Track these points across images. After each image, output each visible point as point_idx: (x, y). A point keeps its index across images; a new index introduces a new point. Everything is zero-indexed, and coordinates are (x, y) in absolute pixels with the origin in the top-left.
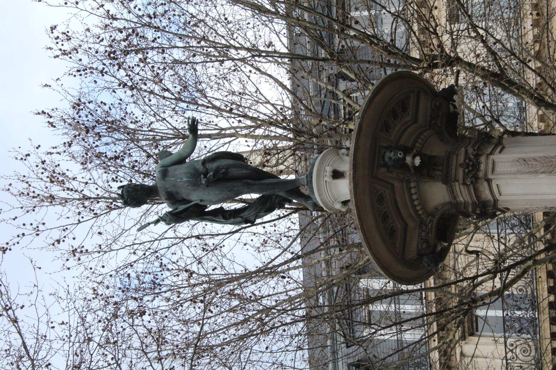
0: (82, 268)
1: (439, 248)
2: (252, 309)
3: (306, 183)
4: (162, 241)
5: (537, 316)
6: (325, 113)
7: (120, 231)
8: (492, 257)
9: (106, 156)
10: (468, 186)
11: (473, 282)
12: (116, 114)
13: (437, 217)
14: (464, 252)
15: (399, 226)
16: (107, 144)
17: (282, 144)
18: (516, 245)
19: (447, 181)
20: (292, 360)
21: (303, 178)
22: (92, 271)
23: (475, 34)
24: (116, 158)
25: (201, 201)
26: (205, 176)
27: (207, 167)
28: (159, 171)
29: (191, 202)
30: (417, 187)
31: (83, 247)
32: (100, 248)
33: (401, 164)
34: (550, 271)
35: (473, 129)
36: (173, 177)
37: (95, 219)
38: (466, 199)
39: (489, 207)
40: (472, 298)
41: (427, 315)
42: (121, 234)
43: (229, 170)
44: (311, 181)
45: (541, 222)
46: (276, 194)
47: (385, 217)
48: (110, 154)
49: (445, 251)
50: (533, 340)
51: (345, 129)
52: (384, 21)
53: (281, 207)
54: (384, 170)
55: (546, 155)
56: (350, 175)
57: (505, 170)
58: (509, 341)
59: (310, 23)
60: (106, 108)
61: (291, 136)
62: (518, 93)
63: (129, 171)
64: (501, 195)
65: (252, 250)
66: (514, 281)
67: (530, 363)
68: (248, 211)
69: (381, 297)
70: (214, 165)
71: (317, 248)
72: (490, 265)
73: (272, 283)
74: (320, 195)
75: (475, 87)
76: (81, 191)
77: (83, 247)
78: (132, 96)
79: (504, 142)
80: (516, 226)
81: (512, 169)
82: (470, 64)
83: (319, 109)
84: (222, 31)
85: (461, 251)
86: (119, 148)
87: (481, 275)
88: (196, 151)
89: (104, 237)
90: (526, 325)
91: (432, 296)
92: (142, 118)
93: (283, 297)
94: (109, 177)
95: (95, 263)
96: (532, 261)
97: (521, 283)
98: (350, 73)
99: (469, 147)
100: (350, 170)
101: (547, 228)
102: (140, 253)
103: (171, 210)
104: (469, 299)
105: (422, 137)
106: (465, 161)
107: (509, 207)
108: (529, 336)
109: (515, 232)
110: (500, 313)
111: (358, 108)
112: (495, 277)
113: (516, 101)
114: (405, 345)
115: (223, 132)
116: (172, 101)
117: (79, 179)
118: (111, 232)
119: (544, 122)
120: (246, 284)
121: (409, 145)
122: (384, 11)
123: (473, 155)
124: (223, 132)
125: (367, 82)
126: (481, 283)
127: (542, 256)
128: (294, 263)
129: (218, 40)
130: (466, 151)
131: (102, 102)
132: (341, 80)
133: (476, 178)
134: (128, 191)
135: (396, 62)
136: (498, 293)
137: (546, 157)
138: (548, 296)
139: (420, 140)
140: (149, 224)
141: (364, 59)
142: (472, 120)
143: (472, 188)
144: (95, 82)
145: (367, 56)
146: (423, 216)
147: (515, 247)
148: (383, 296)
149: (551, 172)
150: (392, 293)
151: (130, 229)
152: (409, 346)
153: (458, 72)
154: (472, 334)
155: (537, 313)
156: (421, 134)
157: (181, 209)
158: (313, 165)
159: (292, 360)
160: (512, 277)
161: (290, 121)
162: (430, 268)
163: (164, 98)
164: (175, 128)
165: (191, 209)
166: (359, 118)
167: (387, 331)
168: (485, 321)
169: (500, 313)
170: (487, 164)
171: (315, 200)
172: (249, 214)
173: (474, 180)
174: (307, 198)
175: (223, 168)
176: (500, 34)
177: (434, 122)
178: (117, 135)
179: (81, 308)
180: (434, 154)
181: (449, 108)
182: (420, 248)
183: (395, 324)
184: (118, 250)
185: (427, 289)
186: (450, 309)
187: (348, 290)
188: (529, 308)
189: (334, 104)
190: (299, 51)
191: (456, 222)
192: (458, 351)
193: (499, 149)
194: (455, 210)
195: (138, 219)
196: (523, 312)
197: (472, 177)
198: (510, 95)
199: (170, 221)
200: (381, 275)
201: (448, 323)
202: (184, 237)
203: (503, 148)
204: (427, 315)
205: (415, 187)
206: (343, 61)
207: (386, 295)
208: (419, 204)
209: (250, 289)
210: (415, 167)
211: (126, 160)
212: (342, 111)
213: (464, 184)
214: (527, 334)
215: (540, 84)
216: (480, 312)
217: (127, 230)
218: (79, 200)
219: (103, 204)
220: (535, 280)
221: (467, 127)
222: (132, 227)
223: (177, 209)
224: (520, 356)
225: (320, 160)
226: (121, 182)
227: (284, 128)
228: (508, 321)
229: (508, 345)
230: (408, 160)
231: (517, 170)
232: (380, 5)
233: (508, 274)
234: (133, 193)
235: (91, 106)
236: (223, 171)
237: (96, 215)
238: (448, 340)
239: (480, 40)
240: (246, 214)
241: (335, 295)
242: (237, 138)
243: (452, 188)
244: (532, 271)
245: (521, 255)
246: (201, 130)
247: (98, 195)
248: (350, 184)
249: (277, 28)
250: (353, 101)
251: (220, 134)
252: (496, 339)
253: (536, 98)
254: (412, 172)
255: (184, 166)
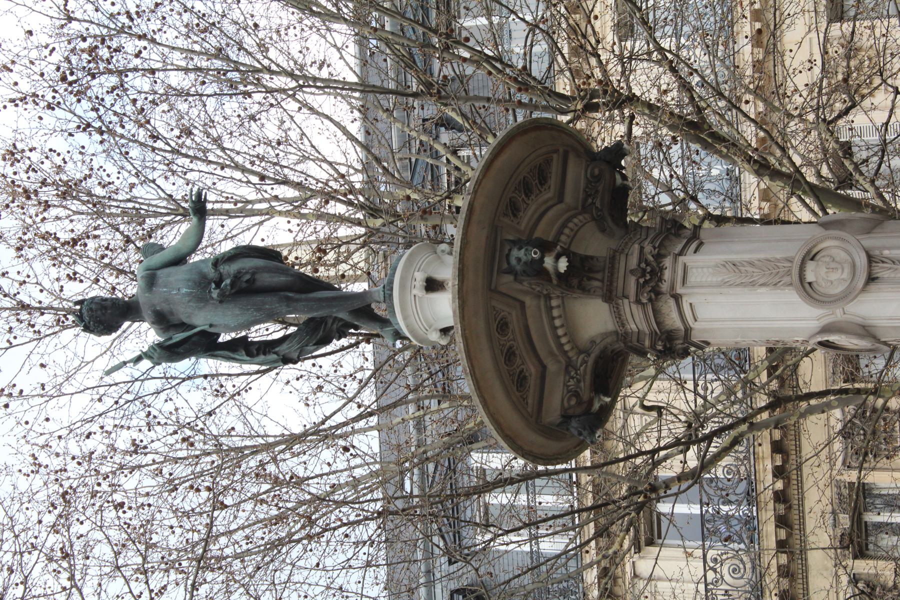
0: (12, 422)
1: (596, 406)
2: (292, 496)
3: (382, 298)
4: (146, 382)
5: (755, 514)
6: (417, 179)
7: (77, 363)
8: (683, 418)
9: (58, 239)
10: (643, 304)
11: (653, 457)
12: (74, 171)
13: (593, 356)
14: (637, 409)
15: (533, 370)
16: (58, 218)
17: (344, 231)
18: (721, 399)
19: (610, 297)
20: (359, 582)
21: (378, 291)
22: (28, 427)
23: (659, 57)
24: (75, 242)
25: (211, 326)
26: (218, 284)
27: (222, 271)
28: (142, 277)
29: (194, 327)
30: (562, 306)
31: (14, 385)
32: (43, 389)
33: (537, 270)
34: (777, 441)
35: (655, 210)
36: (165, 287)
37: (35, 342)
38: (640, 327)
39: (677, 339)
40: (650, 484)
41: (580, 511)
42: (78, 369)
43: (257, 276)
44: (391, 295)
45: (762, 361)
46: (334, 315)
47: (510, 355)
48: (64, 236)
49: (606, 411)
50: (747, 551)
51: (450, 207)
52: (514, 35)
53: (342, 335)
54: (509, 278)
55: (769, 256)
56: (453, 286)
57: (704, 280)
58: (711, 554)
59: (392, 33)
60: (58, 161)
61: (360, 215)
62: (727, 154)
63: (95, 265)
64: (696, 320)
65: (295, 397)
66: (718, 457)
67: (743, 589)
68: (287, 342)
69: (502, 482)
70: (233, 268)
71: (400, 400)
72: (680, 430)
73: (327, 454)
74: (405, 318)
75: (659, 145)
76: (15, 295)
77: (14, 385)
78: (101, 142)
79: (703, 234)
80: (723, 368)
81: (715, 279)
82: (650, 106)
83: (407, 175)
84: (249, 42)
85: (634, 406)
86: (80, 228)
87: (665, 448)
88: (206, 235)
89: (50, 371)
90: (738, 528)
91: (585, 478)
92: (118, 178)
93: (344, 478)
94: (62, 273)
95: (35, 414)
96: (747, 424)
97: (727, 460)
98: (458, 115)
99: (647, 243)
100: (454, 279)
101: (771, 370)
102: (109, 402)
103: (161, 339)
104: (646, 486)
105: (571, 225)
106: (639, 266)
107: (709, 340)
108: (742, 546)
109: (722, 377)
110: (696, 509)
111: (470, 173)
112: (688, 449)
113: (725, 167)
114: (542, 560)
115: (250, 207)
116: (167, 155)
117: (13, 274)
118: (62, 364)
119: (768, 201)
120: (282, 456)
121: (550, 239)
122: (513, 16)
123: (653, 256)
124: (250, 207)
125: (485, 131)
126: (665, 458)
127: (765, 415)
128: (362, 424)
129: (245, 59)
130: (642, 248)
131: (51, 150)
132: (443, 129)
133: (657, 293)
134: (91, 309)
135: (531, 100)
136: (693, 476)
137: (769, 261)
138: (774, 483)
139: (567, 231)
140: (125, 363)
141: (481, 95)
142: (653, 197)
143: (650, 308)
144: (41, 118)
145: (486, 91)
146: (570, 354)
147: (720, 402)
148: (506, 480)
149: (775, 284)
150: (523, 476)
151: (93, 361)
152: (548, 561)
153: (632, 117)
154: (650, 543)
155: (755, 508)
156: (569, 220)
157: (178, 339)
158: (394, 269)
159: (359, 582)
160: (715, 450)
161: (361, 192)
162: (582, 438)
163: (154, 149)
164: (171, 196)
165: (194, 339)
166: (469, 194)
167: (513, 537)
168: (671, 521)
169: (696, 509)
170: (674, 271)
171: (396, 327)
172: (290, 348)
173: (653, 296)
174: (384, 322)
175: (247, 273)
176: (699, 57)
177: (590, 200)
178: (75, 205)
179: (9, 500)
180: (590, 252)
181: (615, 179)
182: (566, 404)
183: (525, 526)
184: (72, 394)
185: (577, 470)
186: (614, 502)
187: (453, 469)
188: (742, 502)
189: (432, 165)
190: (375, 80)
191: (624, 361)
192: (628, 568)
193: (694, 246)
194: (622, 345)
195: (108, 345)
196: (734, 507)
197: (650, 291)
198: (715, 156)
199: (159, 358)
200: (502, 448)
201: (613, 524)
202: (183, 376)
203: (701, 244)
204: (580, 511)
205: (558, 307)
206: (447, 97)
207: (512, 479)
208: (565, 335)
209: (291, 465)
210: (559, 275)
211: (91, 244)
212: (445, 178)
213: (638, 302)
214: (739, 543)
215: (763, 140)
216: (664, 507)
217: (88, 363)
218: (10, 309)
219: (49, 318)
220: (752, 457)
221: (645, 207)
222: (97, 357)
223: (171, 339)
224: (727, 578)
225: (406, 262)
226: (81, 281)
227: (350, 203)
228: (708, 521)
229: (708, 560)
230: (548, 262)
231: (722, 281)
232: (507, 7)
233: (709, 446)
234: (99, 312)
235: (35, 157)
236: (247, 277)
237: (39, 337)
238: (611, 552)
239: (667, 67)
240: (283, 348)
241: (430, 479)
242: (272, 217)
243: (617, 308)
244: (748, 440)
245: (730, 415)
246: (214, 202)
247: (40, 302)
248: (454, 302)
249: (339, 40)
250: (463, 162)
251: (243, 209)
252: (690, 551)
253: (755, 161)
254: (555, 282)
255: (183, 268)
